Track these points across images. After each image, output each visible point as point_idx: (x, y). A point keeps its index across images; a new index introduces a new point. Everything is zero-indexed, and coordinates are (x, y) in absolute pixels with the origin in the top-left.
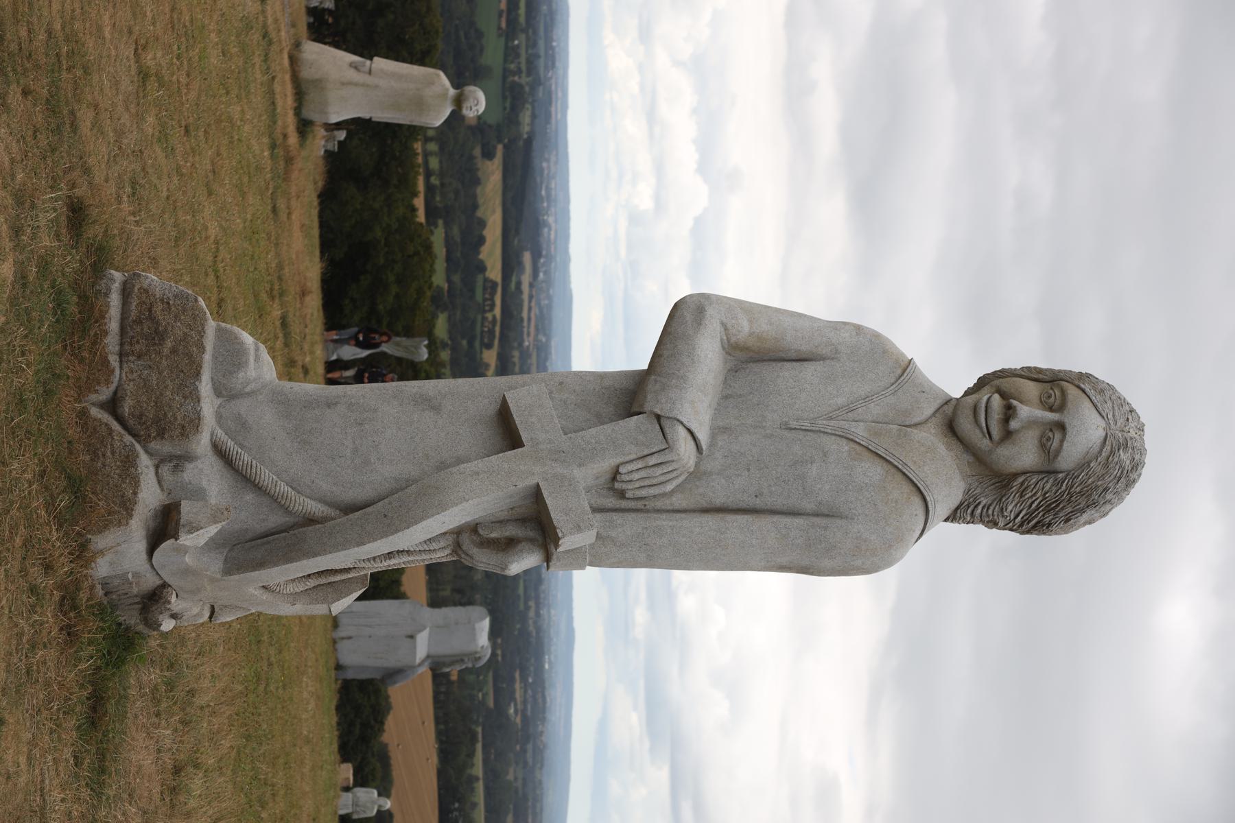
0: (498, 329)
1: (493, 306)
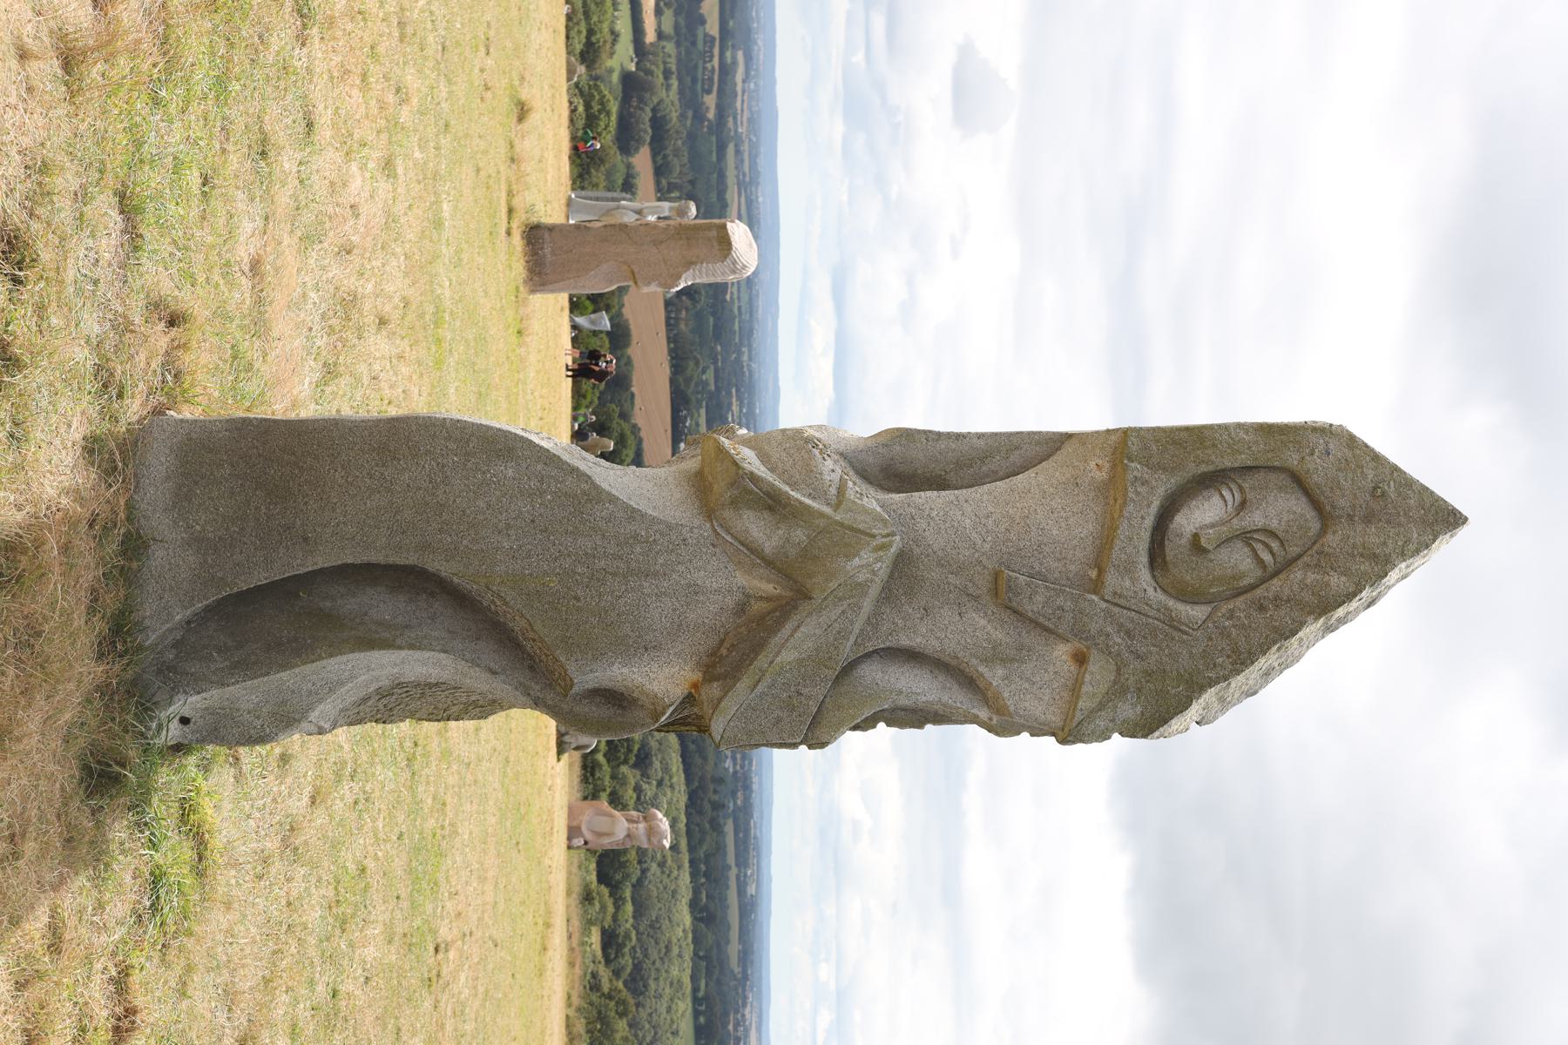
1: (712, 57)
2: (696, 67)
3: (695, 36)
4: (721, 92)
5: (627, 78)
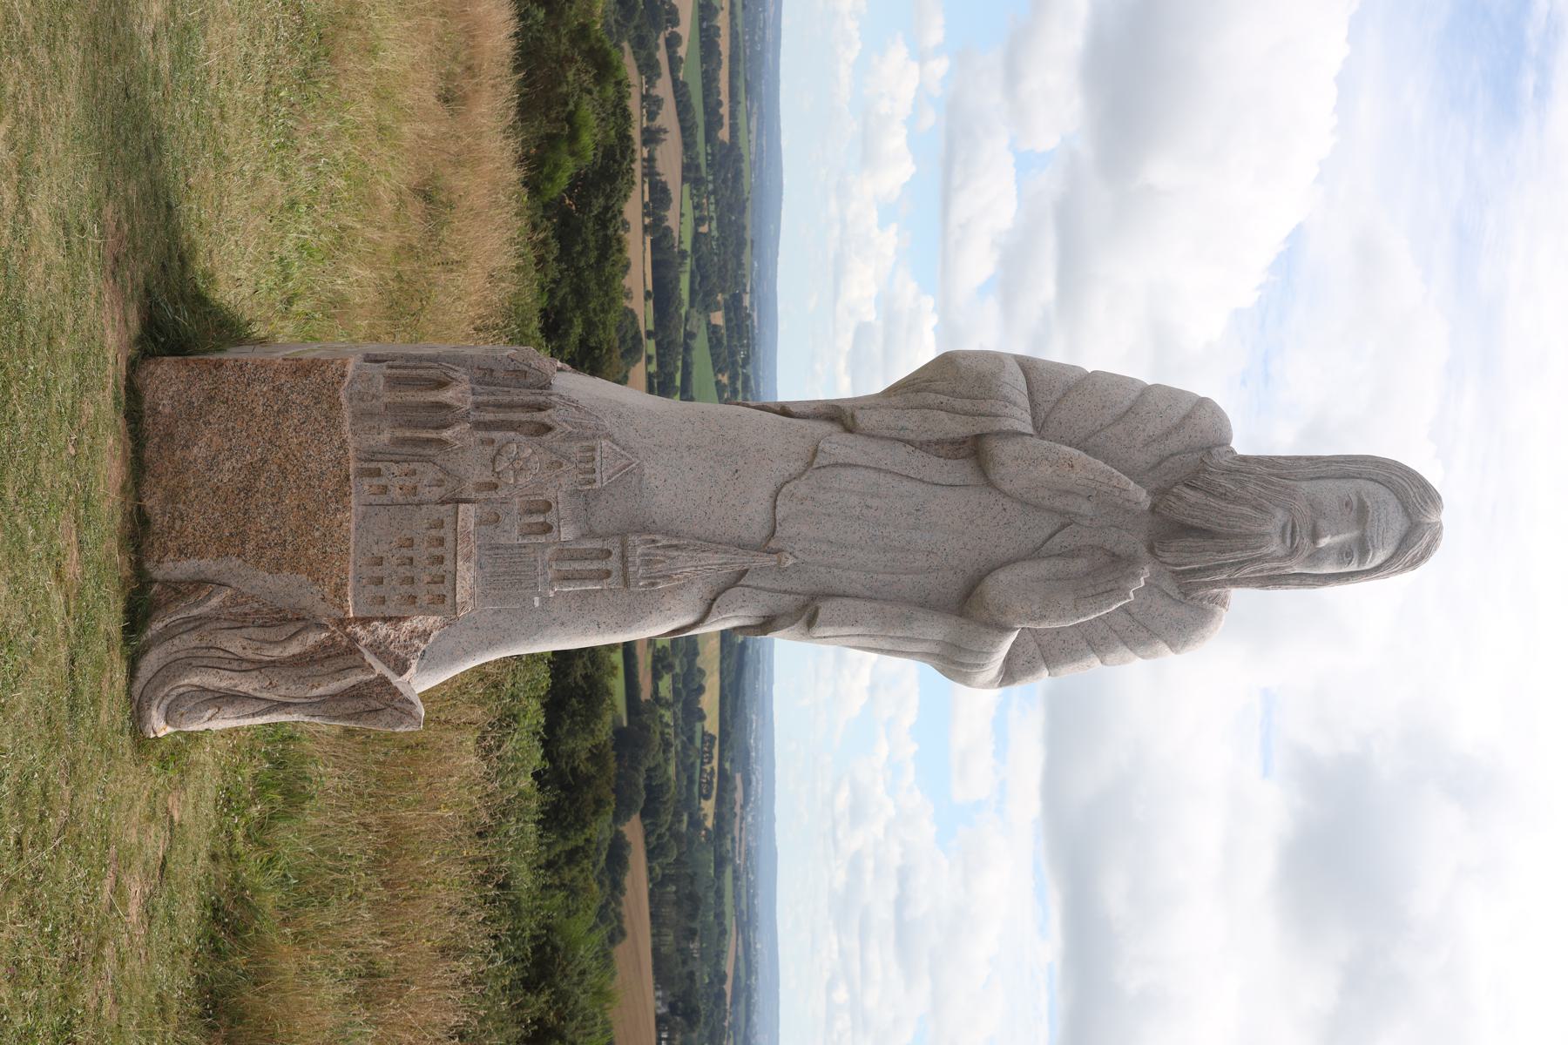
0: (715, 780)
1: (710, 759)
2: (693, 764)
3: (692, 730)
4: (720, 801)
5: (619, 732)
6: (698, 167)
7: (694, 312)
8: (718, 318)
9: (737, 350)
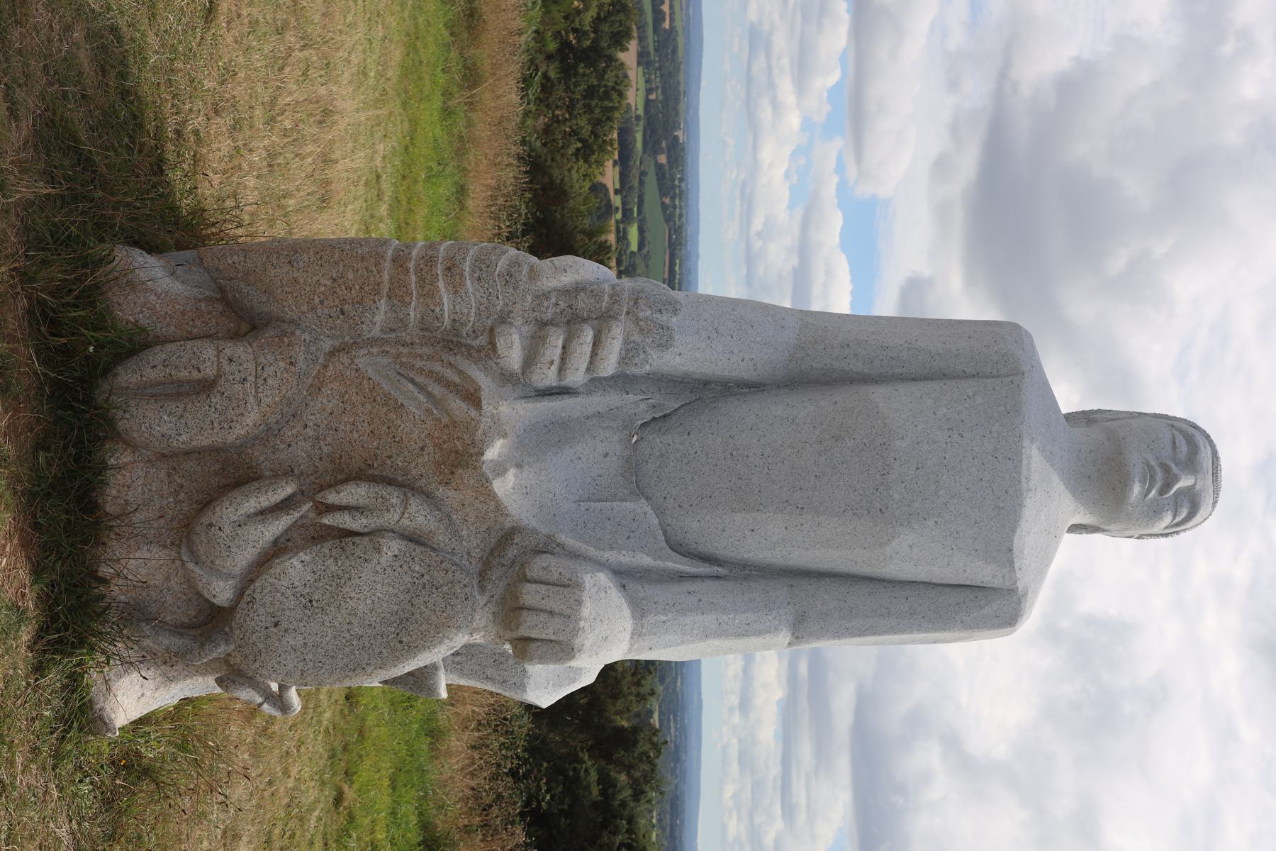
6: (648, 54)
7: (646, 156)
8: (662, 159)
9: (676, 271)
